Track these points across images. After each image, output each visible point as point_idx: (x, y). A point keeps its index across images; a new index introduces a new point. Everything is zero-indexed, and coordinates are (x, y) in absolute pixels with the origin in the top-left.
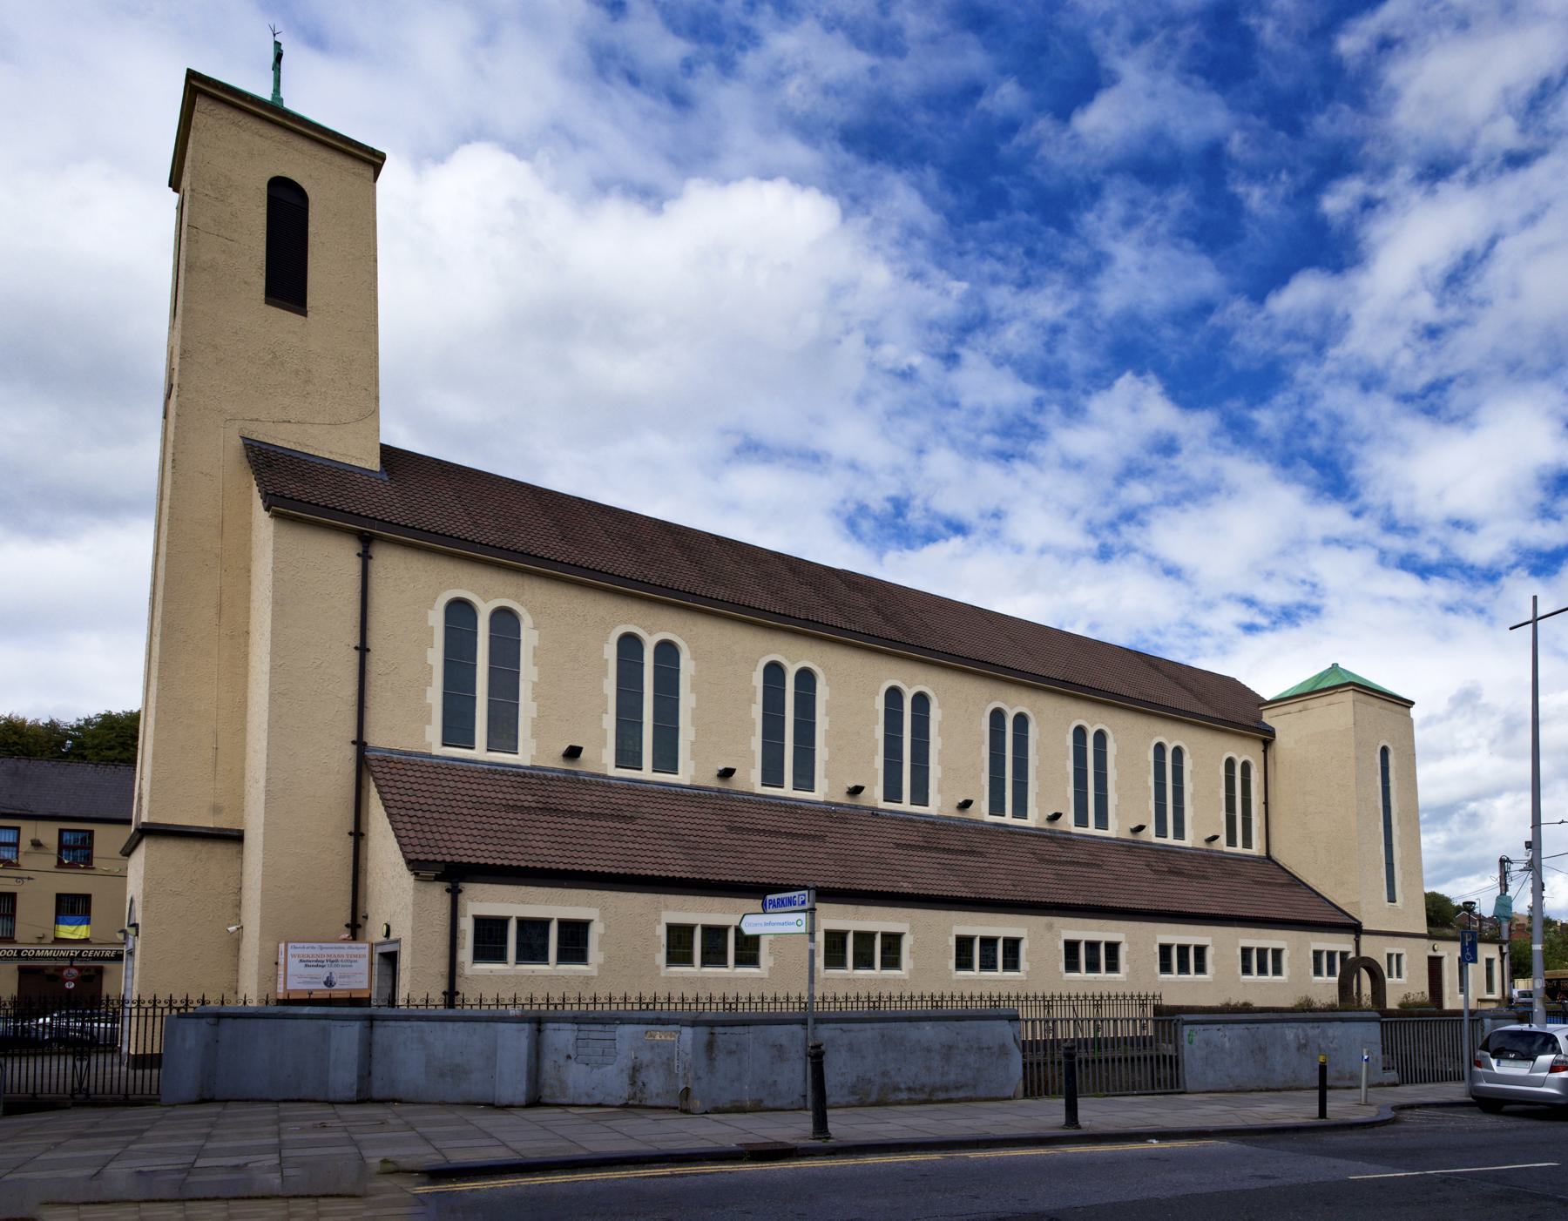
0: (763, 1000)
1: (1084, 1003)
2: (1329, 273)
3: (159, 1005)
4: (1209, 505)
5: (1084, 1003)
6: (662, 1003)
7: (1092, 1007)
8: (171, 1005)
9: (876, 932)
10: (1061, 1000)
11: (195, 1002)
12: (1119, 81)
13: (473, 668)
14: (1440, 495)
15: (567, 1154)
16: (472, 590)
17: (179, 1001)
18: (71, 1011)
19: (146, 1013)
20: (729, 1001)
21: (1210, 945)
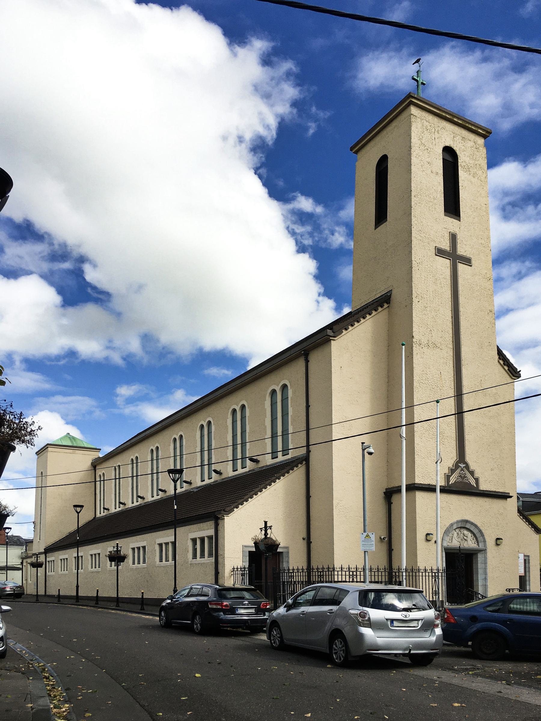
0: (342, 570)
1: (327, 574)
2: (205, 18)
3: (414, 571)
4: (290, 203)
5: (327, 574)
6: (338, 571)
7: (430, 578)
8: (432, 571)
9: (204, 537)
10: (328, 571)
11: (429, 570)
12: (28, 221)
13: (402, 391)
14: (267, 127)
15: (459, 659)
16: (267, 391)
17: (396, 569)
18: (311, 571)
19: (426, 574)
20: (428, 571)
21: (189, 539)
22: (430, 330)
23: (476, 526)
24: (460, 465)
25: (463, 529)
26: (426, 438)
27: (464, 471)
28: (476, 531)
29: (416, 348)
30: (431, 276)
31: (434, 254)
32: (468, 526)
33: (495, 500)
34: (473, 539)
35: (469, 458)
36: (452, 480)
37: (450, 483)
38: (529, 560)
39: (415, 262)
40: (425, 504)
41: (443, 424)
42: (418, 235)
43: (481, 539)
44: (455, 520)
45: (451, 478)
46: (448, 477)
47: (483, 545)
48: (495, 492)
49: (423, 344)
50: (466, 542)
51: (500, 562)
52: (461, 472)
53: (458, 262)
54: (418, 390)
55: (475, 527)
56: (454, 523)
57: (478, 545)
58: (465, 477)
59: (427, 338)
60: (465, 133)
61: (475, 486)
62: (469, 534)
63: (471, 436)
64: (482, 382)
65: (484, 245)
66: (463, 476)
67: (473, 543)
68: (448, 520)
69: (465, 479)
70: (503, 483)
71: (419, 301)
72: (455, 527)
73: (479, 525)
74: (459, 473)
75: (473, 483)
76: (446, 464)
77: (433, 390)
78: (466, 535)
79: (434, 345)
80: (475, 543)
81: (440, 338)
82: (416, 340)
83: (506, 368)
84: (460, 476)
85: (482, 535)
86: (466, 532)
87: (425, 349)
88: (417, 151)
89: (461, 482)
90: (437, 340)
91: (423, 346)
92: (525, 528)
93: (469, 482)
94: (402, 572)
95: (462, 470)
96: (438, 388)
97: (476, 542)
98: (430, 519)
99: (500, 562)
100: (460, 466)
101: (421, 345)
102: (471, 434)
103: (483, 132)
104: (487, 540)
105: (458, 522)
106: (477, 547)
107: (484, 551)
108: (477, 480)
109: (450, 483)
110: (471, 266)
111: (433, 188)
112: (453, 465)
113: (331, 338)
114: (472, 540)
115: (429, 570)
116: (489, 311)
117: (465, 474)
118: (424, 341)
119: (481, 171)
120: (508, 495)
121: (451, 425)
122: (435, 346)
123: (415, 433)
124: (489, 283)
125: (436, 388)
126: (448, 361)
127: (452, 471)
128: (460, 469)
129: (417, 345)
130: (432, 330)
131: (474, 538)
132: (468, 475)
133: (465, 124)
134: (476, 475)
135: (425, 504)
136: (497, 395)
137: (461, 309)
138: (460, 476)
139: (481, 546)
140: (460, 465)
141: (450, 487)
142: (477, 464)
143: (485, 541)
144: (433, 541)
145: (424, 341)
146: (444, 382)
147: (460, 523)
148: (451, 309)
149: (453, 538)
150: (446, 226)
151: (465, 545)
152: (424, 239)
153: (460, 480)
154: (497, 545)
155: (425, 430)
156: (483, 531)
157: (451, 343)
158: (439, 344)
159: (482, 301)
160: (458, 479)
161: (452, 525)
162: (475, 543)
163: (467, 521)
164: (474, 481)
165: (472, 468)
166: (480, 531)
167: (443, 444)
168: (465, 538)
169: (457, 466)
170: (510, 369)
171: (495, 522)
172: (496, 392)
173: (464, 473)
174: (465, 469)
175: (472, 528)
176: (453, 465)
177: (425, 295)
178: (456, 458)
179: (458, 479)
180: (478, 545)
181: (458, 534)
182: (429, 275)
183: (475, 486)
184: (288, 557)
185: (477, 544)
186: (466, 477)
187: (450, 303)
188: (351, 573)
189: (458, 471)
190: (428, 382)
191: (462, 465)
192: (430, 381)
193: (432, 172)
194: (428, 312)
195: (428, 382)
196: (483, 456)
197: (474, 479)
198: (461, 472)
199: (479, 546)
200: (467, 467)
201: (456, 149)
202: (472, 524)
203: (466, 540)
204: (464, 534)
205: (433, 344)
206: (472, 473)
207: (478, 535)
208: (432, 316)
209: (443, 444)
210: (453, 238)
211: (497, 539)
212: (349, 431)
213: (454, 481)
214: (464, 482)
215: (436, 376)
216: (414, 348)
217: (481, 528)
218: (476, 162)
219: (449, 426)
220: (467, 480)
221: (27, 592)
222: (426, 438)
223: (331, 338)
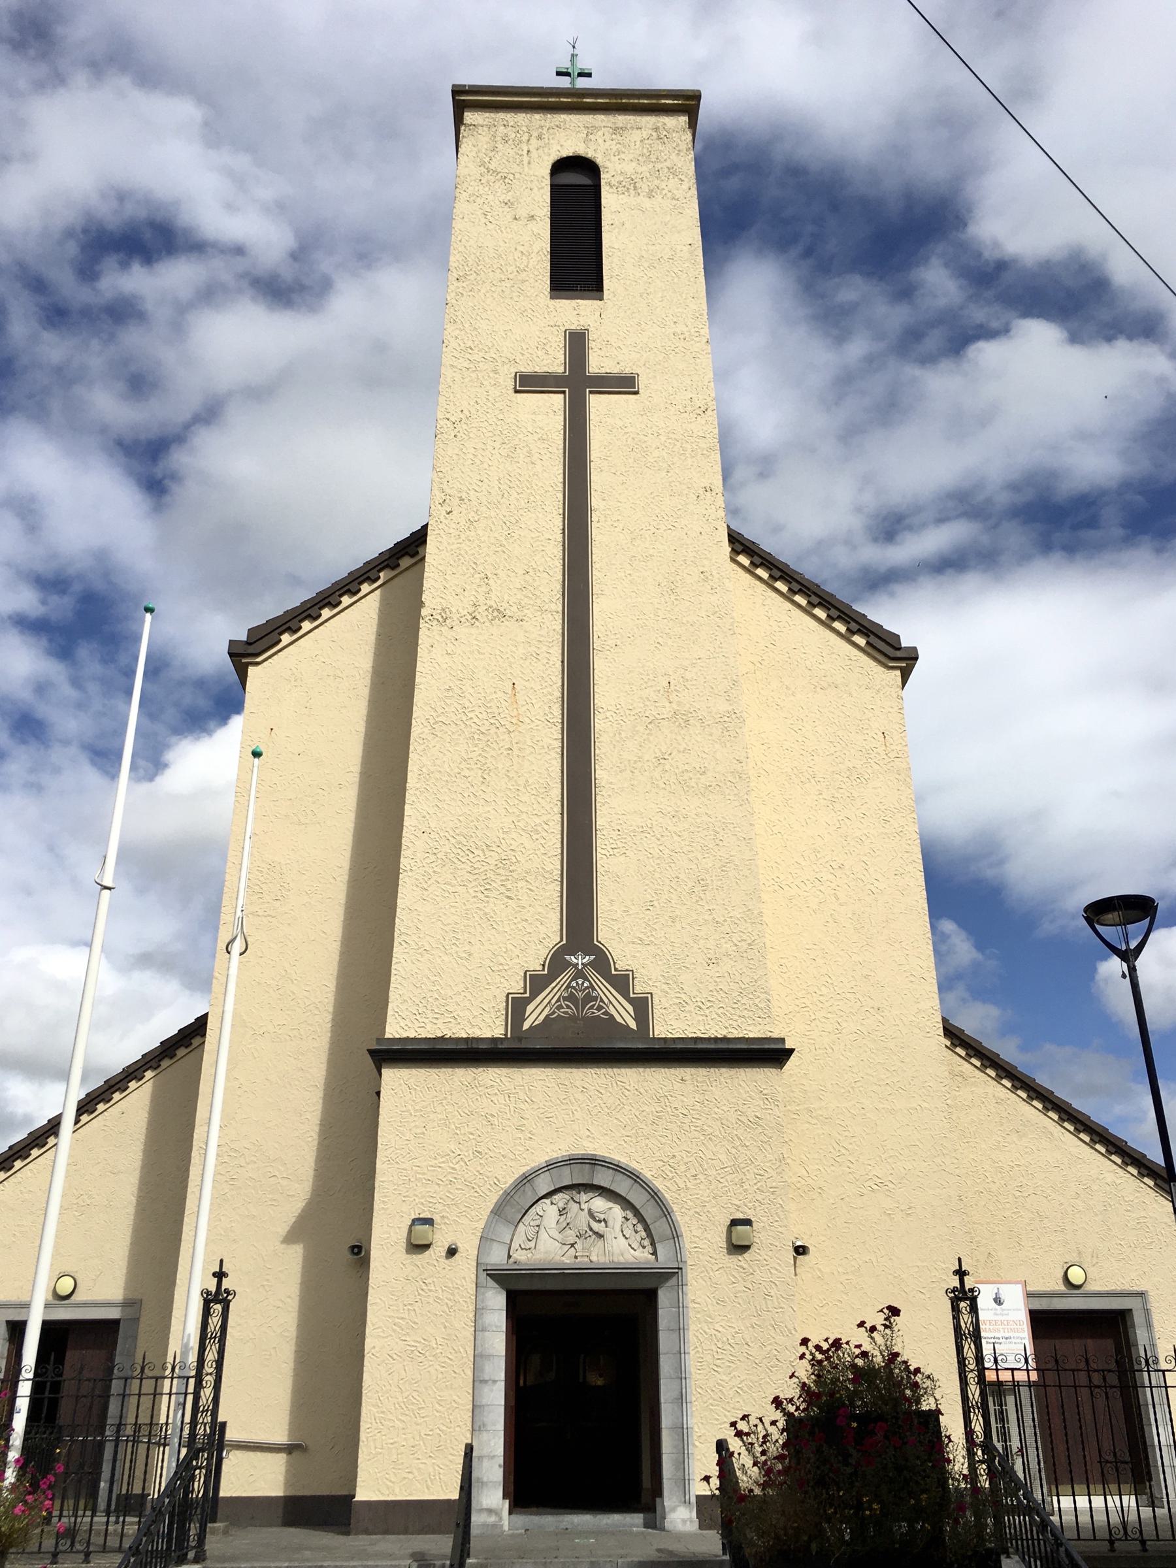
23: (635, 1177)
25: (591, 1195)
28: (637, 1197)
29: (427, 633)
30: (497, 445)
31: (511, 391)
32: (603, 1178)
33: (723, 1070)
35: (606, 933)
36: (535, 1015)
37: (526, 1026)
38: (1147, 1312)
40: (416, 1111)
41: (514, 835)
44: (541, 1159)
45: (530, 1008)
46: (517, 1007)
50: (601, 1243)
53: (591, 392)
55: (630, 1181)
57: (655, 1253)
58: (589, 998)
60: (621, 119)
61: (633, 1025)
62: (617, 1212)
63: (622, 858)
66: (580, 995)
68: (509, 1163)
71: (451, 512)
72: (544, 1184)
73: (647, 1174)
74: (569, 986)
75: (624, 1014)
76: (517, 961)
77: (482, 737)
78: (602, 1217)
80: (644, 1247)
81: (515, 591)
83: (860, 640)
84: (571, 998)
86: (599, 1204)
87: (462, 631)
89: (573, 1018)
90: (506, 597)
92: (1110, 1178)
93: (606, 1013)
94: (1163, 1371)
95: (580, 974)
96: (502, 729)
97: (646, 1242)
98: (433, 1162)
100: (569, 964)
101: (448, 622)
102: (623, 850)
104: (684, 1230)
105: (551, 1166)
106: (648, 1262)
107: (671, 1275)
108: (642, 1007)
109: (526, 1026)
110: (636, 393)
111: (516, 249)
112: (545, 962)
114: (628, 1233)
115: (1011, 1358)
116: (701, 491)
118: (460, 606)
120: (780, 1046)
122: (500, 614)
123: (401, 876)
124: (702, 421)
127: (537, 983)
128: (570, 972)
130: (489, 576)
131: (640, 1227)
132: (605, 991)
133: (619, 101)
134: (639, 988)
135: (416, 1111)
136: (734, 716)
137: (596, 501)
138: (571, 998)
141: (520, 1039)
142: (649, 948)
143: (675, 1236)
144: (439, 1249)
145: (460, 606)
147: (566, 1171)
150: (555, 319)
151: (594, 1258)
153: (568, 1009)
154: (738, 1248)
156: (668, 1196)
157: (559, 596)
161: (526, 1180)
164: (630, 1009)
166: (655, 1196)
167: (509, 897)
169: (557, 963)
170: (873, 639)
171: (723, 1157)
172: (730, 709)
175: (622, 1186)
176: (545, 962)
180: (655, 1253)
182: (490, 442)
183: (633, 1025)
185: (650, 1249)
186: (595, 999)
187: (560, 496)
188: (1097, 1379)
189: (564, 978)
191: (579, 960)
192: (471, 715)
197: (631, 1001)
200: (602, 962)
202: (618, 1168)
204: (591, 1214)
205: (490, 610)
206: (622, 983)
207: (649, 1212)
209: (509, 897)
210: (577, 343)
211: (735, 1223)
212: (277, 904)
213: (542, 1017)
214: (583, 1018)
216: (423, 633)
217: (658, 1184)
220: (599, 1008)
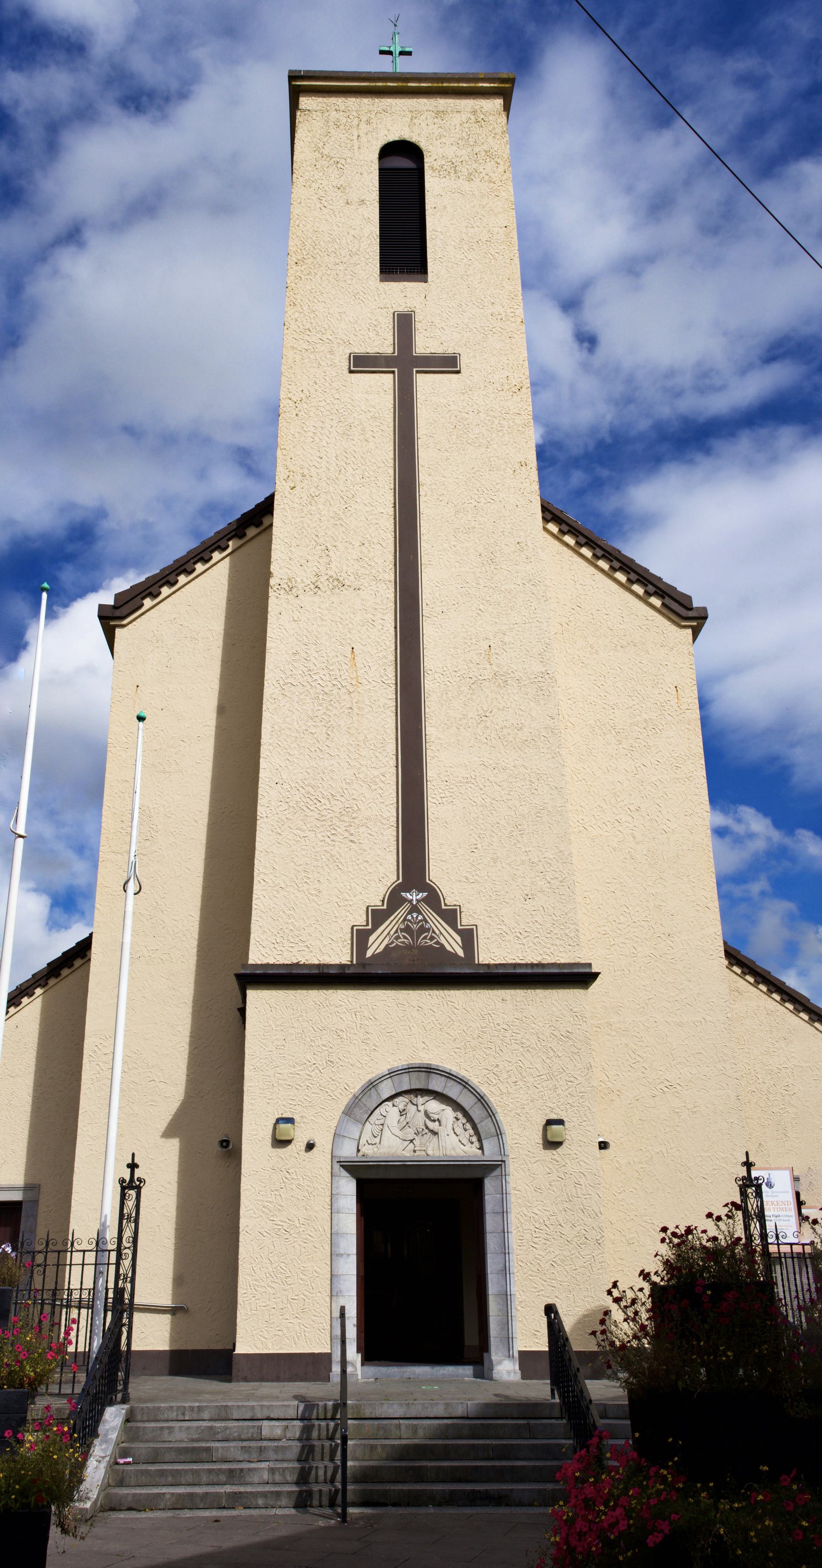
22: (324, 547)
23: (464, 1084)
24: (408, 896)
25: (426, 1098)
26: (296, 832)
27: (419, 913)
28: (467, 1101)
29: (276, 601)
30: (334, 423)
31: (347, 371)
32: (437, 1084)
34: (465, 1130)
36: (376, 944)
37: (369, 954)
39: (290, 402)
42: (301, 342)
43: (485, 1126)
44: (384, 1069)
45: (372, 938)
46: (361, 937)
47: (496, 1149)
48: (540, 965)
49: (301, 586)
50: (435, 1138)
51: (566, 1205)
52: (409, 917)
53: (418, 372)
54: (275, 706)
56: (381, 1079)
57: (481, 1148)
58: (423, 930)
59: (315, 568)
60: (442, 103)
62: (448, 1114)
64: (493, 651)
65: (499, 317)
66: (415, 927)
67: (465, 1141)
69: (425, 938)
70: (572, 935)
72: (387, 1089)
74: (405, 919)
75: (453, 944)
78: (436, 1117)
79: (336, 583)
80: (472, 1143)
82: (278, 581)
83: (656, 602)
84: (407, 930)
85: (491, 1114)
86: (434, 1106)
88: (307, 174)
89: (409, 947)
90: (345, 568)
91: (300, 592)
93: (438, 943)
95: (414, 909)
97: (474, 1139)
99: (566, 1205)
100: (405, 900)
102: (451, 799)
103: (492, 85)
105: (392, 1074)
106: (476, 1156)
108: (468, 937)
109: (369, 954)
110: (458, 372)
113: (112, 623)
116: (517, 466)
117: (425, 920)
119: (493, 163)
120: (587, 970)
121: (382, 785)
125: (335, 692)
126: (379, 615)
127: (378, 917)
128: (406, 907)
129: (282, 592)
130: (330, 547)
131: (468, 1126)
132: (436, 923)
134: (465, 921)
135: (277, 1026)
136: (547, 676)
138: (407, 930)
139: (490, 1152)
140: (408, 896)
143: (499, 1133)
144: (299, 1144)
146: (362, 671)
147: (405, 1078)
148: (392, 486)
149: (386, 1129)
151: (430, 1152)
152: (318, 346)
153: (405, 940)
155: (291, 809)
158: (352, 578)
159: (495, 446)
160: (398, 938)
161: (372, 1085)
162: (472, 1143)
163: (429, 1070)
165: (450, 897)
166: (481, 1099)
167: (352, 841)
168: (431, 1125)
169: (395, 899)
170: (668, 601)
173: (420, 917)
174: (424, 907)
175: (453, 1091)
177: (313, 469)
178: (431, 878)
179: (398, 938)
180: (481, 1148)
181: (402, 1113)
183: (461, 953)
184: (35, 1216)
185: (477, 1144)
186: (428, 930)
189: (401, 913)
190: (310, 680)
191: (414, 896)
192: (315, 677)
193: (348, 203)
194: (321, 507)
195: (310, 680)
196: (495, 860)
198: (409, 917)
199: (483, 1154)
200: (433, 899)
201: (418, 139)
202: (449, 1076)
203: (435, 1133)
205: (331, 580)
206: (451, 916)
207: (477, 1113)
208: (331, 515)
209: (352, 841)
211: (550, 1122)
212: (148, 843)
215: (336, 660)
217: (484, 1089)
218: (477, 149)
219: (373, 787)
220: (432, 938)
221: (129, 1344)
222: (296, 832)
223: (112, 623)
